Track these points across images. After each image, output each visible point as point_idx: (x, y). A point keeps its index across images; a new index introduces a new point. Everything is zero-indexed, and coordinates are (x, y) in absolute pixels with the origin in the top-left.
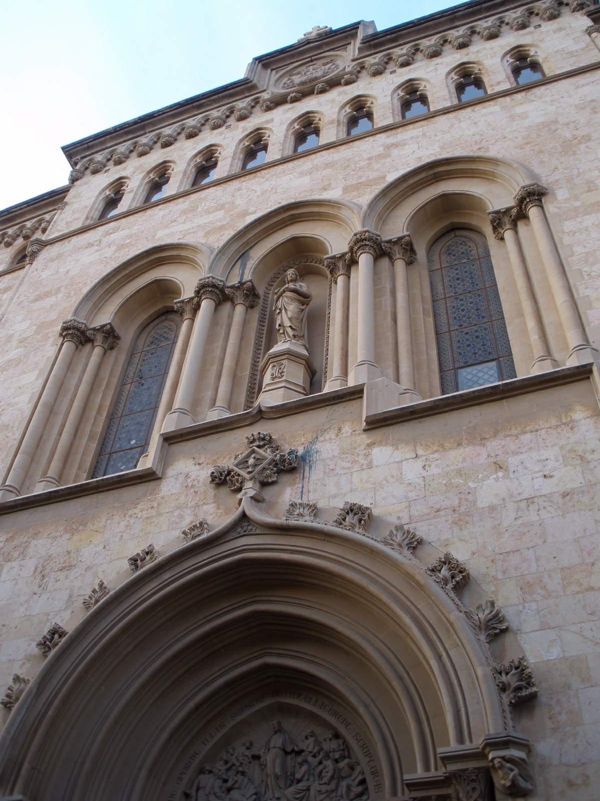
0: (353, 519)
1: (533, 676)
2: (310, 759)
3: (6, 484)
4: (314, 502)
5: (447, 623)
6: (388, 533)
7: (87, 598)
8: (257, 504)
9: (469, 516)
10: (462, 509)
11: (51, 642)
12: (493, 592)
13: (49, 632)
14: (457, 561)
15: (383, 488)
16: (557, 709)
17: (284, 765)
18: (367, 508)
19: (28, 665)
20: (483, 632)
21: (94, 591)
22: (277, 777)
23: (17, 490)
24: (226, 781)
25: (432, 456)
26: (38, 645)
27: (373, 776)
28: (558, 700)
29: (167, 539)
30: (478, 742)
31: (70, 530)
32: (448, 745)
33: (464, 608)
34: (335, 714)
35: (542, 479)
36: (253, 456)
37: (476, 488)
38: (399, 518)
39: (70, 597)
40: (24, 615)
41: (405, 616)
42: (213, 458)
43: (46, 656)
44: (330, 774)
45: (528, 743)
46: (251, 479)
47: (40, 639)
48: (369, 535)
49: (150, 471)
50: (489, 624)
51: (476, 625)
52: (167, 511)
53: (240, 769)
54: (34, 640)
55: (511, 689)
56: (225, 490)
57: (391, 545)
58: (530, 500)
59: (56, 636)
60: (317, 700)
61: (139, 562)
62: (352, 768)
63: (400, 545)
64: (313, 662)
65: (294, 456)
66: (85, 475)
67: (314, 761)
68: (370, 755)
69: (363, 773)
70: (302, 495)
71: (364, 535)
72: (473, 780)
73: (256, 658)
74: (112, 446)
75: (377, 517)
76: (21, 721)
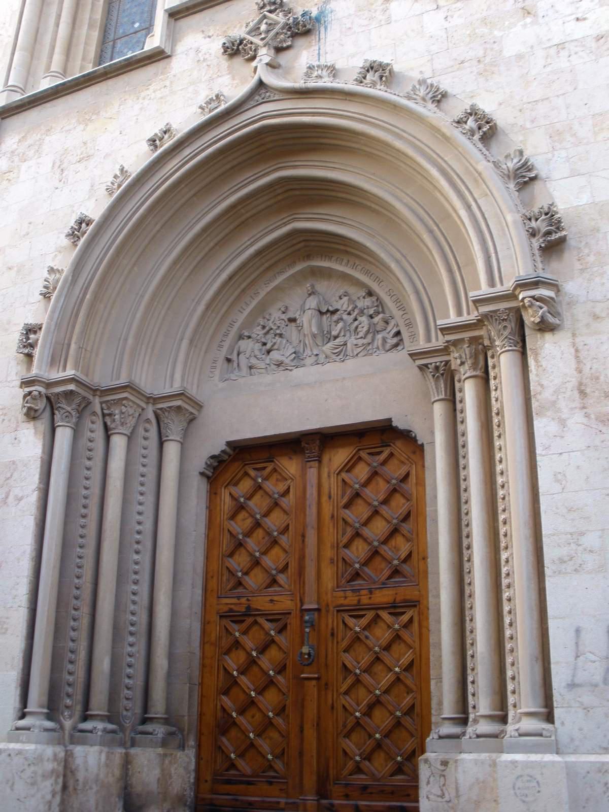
0: (374, 77)
1: (562, 221)
2: (345, 317)
3: (9, 84)
4: (333, 63)
5: (475, 173)
6: (411, 88)
7: (110, 185)
8: (273, 70)
9: (495, 66)
10: (488, 60)
11: (79, 232)
12: (521, 142)
13: (76, 222)
14: (484, 112)
15: (403, 43)
16: (586, 251)
17: (320, 326)
18: (388, 65)
19: (60, 257)
20: (512, 181)
21: (116, 177)
22: (314, 336)
23: (21, 89)
24: (265, 344)
25: (454, 6)
26: (67, 236)
27: (408, 327)
28: (587, 243)
29: (184, 117)
30: (509, 285)
31: (83, 121)
32: (480, 288)
33: (492, 158)
34: (367, 273)
35: (575, 21)
36: (265, 21)
37: (502, 36)
38: (421, 72)
39: (92, 186)
40: (48, 210)
41: (432, 169)
42: (224, 29)
43: (76, 245)
44: (365, 329)
45: (557, 283)
46: (265, 46)
47: (68, 230)
48: (392, 91)
49: (158, 50)
50: (518, 172)
51: (504, 174)
52: (180, 88)
53: (278, 332)
54: (61, 233)
55: (541, 234)
56: (238, 61)
57: (415, 99)
58: (561, 46)
59: (84, 225)
60: (348, 261)
61: (158, 142)
62: (387, 323)
63: (424, 99)
64: (342, 223)
65: (308, 17)
66: (91, 65)
67: (349, 319)
68: (403, 308)
69: (398, 326)
70: (319, 57)
71: (386, 91)
72: (503, 320)
73: (285, 224)
74: (115, 32)
75: (398, 73)
76: (62, 307)
